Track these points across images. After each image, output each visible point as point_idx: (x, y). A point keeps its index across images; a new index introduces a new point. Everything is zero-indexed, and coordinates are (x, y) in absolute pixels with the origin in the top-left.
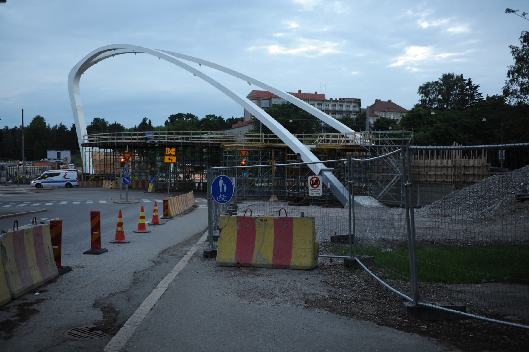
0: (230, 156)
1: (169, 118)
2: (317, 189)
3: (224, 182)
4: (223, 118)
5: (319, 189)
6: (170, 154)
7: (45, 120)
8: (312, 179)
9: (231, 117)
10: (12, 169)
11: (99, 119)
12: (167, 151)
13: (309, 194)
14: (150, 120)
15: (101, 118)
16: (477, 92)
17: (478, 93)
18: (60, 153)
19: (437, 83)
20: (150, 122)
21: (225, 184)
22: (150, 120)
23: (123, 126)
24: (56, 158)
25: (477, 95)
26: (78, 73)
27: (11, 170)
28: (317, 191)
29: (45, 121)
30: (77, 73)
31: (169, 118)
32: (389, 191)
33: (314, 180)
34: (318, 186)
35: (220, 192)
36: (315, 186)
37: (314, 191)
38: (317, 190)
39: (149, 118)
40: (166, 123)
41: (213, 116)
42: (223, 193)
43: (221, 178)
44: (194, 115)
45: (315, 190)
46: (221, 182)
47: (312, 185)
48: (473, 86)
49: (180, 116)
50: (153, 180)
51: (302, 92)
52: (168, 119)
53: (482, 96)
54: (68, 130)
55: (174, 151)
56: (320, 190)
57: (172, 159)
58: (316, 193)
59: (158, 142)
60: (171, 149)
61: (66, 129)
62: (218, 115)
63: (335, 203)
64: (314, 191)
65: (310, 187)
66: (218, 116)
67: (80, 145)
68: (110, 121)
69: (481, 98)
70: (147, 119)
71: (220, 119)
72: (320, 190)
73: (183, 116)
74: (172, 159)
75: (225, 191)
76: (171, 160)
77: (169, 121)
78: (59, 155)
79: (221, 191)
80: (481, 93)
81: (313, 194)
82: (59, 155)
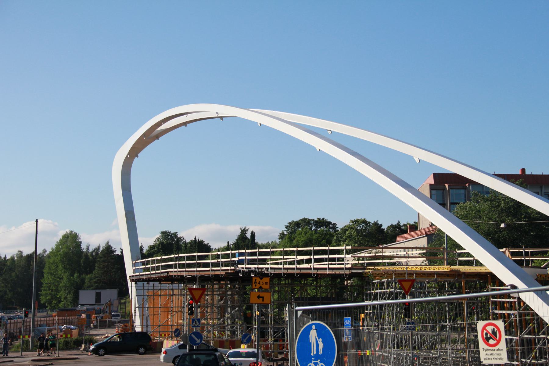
0: (383, 291)
1: (287, 227)
2: (496, 348)
3: (319, 335)
4: (381, 225)
5: (500, 348)
7: (80, 238)
8: (484, 328)
9: (395, 223)
10: (14, 323)
11: (170, 232)
12: (255, 283)
13: (482, 359)
14: (252, 232)
15: (172, 231)
18: (100, 293)
20: (253, 235)
21: (321, 339)
22: (252, 232)
23: (208, 244)
24: (94, 302)
26: (128, 156)
27: (12, 325)
28: (496, 352)
29: (80, 240)
30: (127, 156)
31: (287, 227)
33: (490, 329)
34: (498, 342)
35: (312, 354)
36: (491, 342)
37: (490, 352)
38: (497, 350)
39: (251, 228)
40: (282, 236)
41: (364, 222)
42: (317, 357)
43: (314, 327)
44: (329, 220)
45: (492, 350)
46: (313, 334)
47: (487, 340)
49: (306, 222)
50: (247, 338)
51: (527, 173)
52: (285, 229)
54: (116, 253)
55: (266, 283)
56: (502, 350)
57: (263, 298)
58: (496, 357)
59: (255, 268)
60: (261, 279)
61: (114, 251)
62: (371, 220)
63: (239, 329)
64: (490, 352)
65: (482, 344)
66: (372, 222)
67: (128, 278)
68: (187, 235)
70: (247, 230)
71: (377, 226)
72: (502, 350)
73: (311, 224)
74: (263, 298)
75: (321, 353)
76: (261, 299)
77: (286, 233)
79: (313, 352)
81: (488, 359)
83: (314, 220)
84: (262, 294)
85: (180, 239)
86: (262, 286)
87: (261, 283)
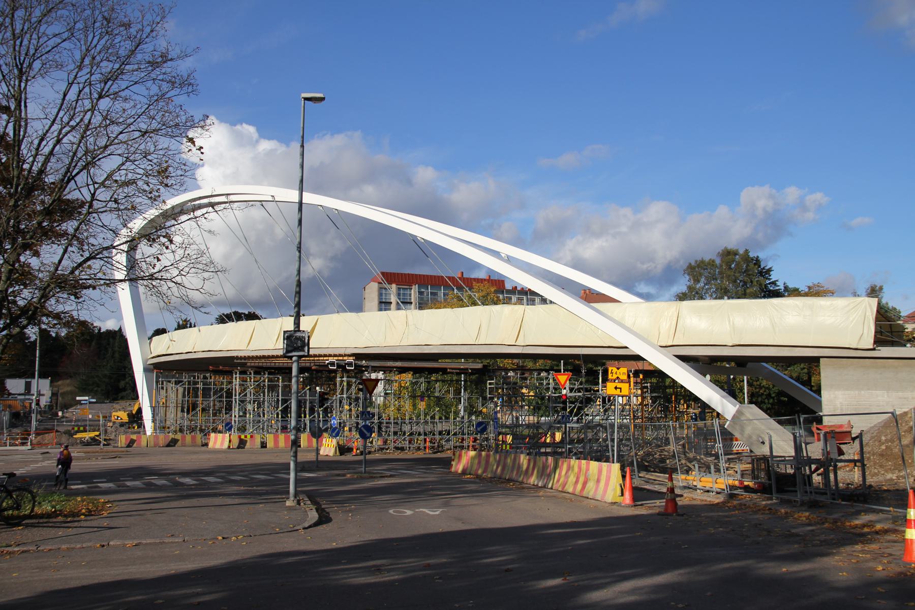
6: (618, 378)
16: (770, 279)
17: (771, 281)
18: (30, 382)
19: (712, 263)
25: (770, 283)
32: (771, 494)
48: (764, 268)
50: (481, 427)
53: (779, 286)
55: (624, 373)
57: (621, 388)
60: (618, 369)
69: (777, 288)
74: (621, 388)
76: (619, 390)
78: (28, 386)
80: (777, 281)
82: (28, 386)
83: (244, 314)
84: (619, 385)
85: (115, 331)
86: (619, 376)
87: (618, 373)
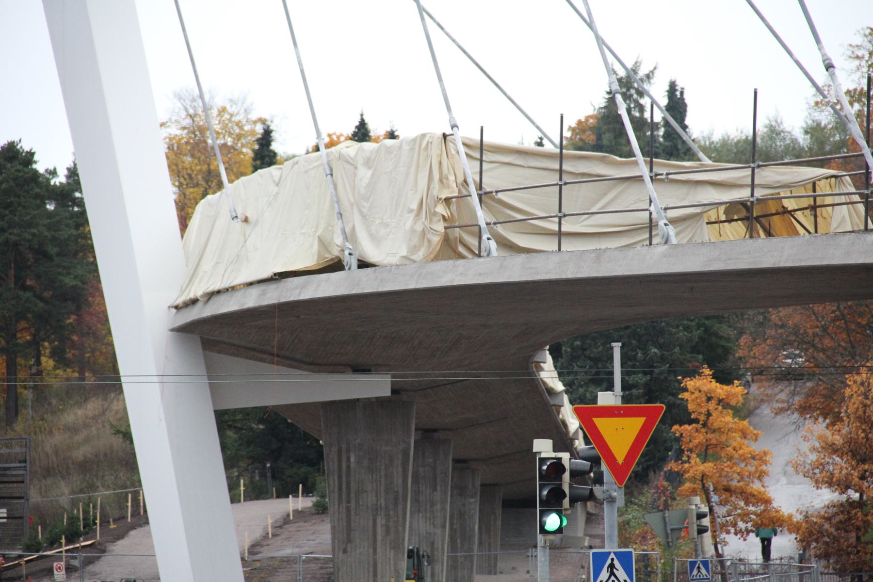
14: (673, 87)
22: (673, 87)
